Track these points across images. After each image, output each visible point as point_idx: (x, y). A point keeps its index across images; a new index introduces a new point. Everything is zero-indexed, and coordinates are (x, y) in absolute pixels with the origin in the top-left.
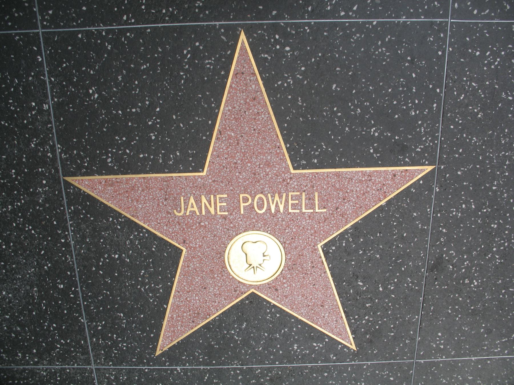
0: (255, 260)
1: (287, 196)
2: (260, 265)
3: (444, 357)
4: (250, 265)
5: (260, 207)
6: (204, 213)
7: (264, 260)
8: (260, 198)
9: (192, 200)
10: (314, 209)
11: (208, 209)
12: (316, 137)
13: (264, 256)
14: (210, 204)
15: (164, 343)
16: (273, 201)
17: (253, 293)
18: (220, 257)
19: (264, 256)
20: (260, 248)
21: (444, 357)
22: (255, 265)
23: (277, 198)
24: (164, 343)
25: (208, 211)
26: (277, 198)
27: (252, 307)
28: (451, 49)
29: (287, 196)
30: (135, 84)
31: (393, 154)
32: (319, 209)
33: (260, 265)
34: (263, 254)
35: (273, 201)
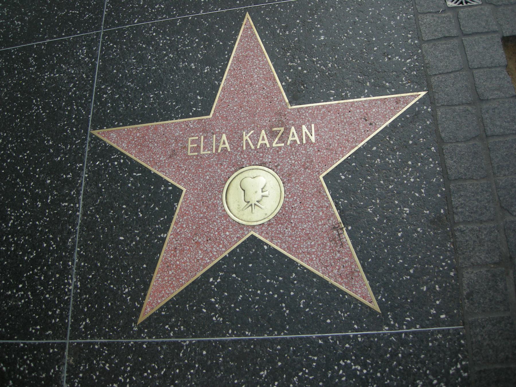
0: (256, 197)
2: (258, 201)
3: (418, 326)
6: (304, 142)
7: (263, 196)
9: (293, 130)
10: (199, 151)
11: (309, 137)
12: (194, 97)
13: (262, 192)
14: (306, 135)
17: (252, 235)
19: (262, 192)
21: (418, 326)
22: (254, 201)
27: (252, 256)
28: (190, 18)
33: (258, 201)
34: (262, 189)
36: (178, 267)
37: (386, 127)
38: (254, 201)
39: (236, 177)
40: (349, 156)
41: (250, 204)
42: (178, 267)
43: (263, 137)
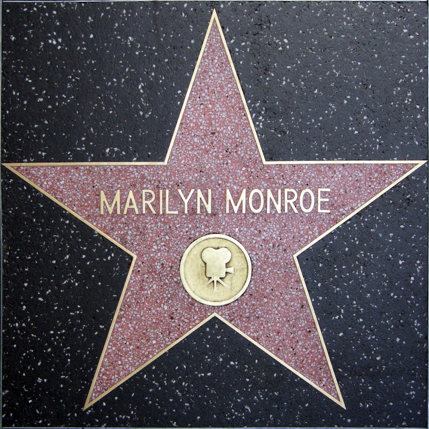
0: (215, 274)
1: (283, 193)
2: (221, 278)
4: (210, 278)
5: (307, 205)
6: (286, 211)
8: (257, 194)
9: (131, 195)
11: (121, 203)
13: (227, 267)
15: (95, 394)
16: (241, 207)
18: (185, 248)
20: (224, 255)
22: (216, 278)
23: (236, 209)
24: (95, 394)
25: (275, 194)
26: (236, 209)
29: (283, 193)
30: (93, 145)
31: (102, 17)
32: (288, 192)
33: (221, 278)
35: (241, 207)
36: (124, 355)
37: (328, 159)
38: (216, 278)
39: (227, 241)
40: (349, 220)
41: (211, 280)
42: (124, 355)
43: (131, 200)
